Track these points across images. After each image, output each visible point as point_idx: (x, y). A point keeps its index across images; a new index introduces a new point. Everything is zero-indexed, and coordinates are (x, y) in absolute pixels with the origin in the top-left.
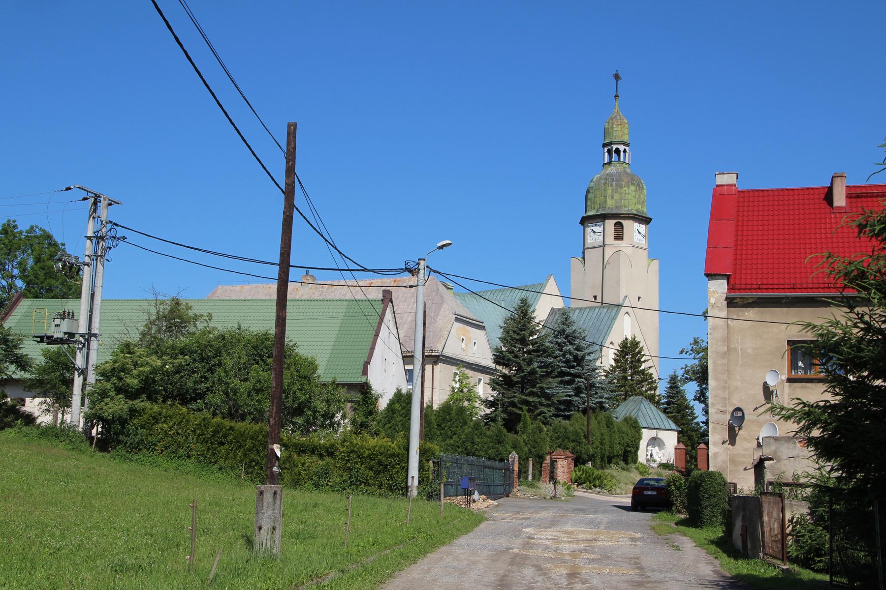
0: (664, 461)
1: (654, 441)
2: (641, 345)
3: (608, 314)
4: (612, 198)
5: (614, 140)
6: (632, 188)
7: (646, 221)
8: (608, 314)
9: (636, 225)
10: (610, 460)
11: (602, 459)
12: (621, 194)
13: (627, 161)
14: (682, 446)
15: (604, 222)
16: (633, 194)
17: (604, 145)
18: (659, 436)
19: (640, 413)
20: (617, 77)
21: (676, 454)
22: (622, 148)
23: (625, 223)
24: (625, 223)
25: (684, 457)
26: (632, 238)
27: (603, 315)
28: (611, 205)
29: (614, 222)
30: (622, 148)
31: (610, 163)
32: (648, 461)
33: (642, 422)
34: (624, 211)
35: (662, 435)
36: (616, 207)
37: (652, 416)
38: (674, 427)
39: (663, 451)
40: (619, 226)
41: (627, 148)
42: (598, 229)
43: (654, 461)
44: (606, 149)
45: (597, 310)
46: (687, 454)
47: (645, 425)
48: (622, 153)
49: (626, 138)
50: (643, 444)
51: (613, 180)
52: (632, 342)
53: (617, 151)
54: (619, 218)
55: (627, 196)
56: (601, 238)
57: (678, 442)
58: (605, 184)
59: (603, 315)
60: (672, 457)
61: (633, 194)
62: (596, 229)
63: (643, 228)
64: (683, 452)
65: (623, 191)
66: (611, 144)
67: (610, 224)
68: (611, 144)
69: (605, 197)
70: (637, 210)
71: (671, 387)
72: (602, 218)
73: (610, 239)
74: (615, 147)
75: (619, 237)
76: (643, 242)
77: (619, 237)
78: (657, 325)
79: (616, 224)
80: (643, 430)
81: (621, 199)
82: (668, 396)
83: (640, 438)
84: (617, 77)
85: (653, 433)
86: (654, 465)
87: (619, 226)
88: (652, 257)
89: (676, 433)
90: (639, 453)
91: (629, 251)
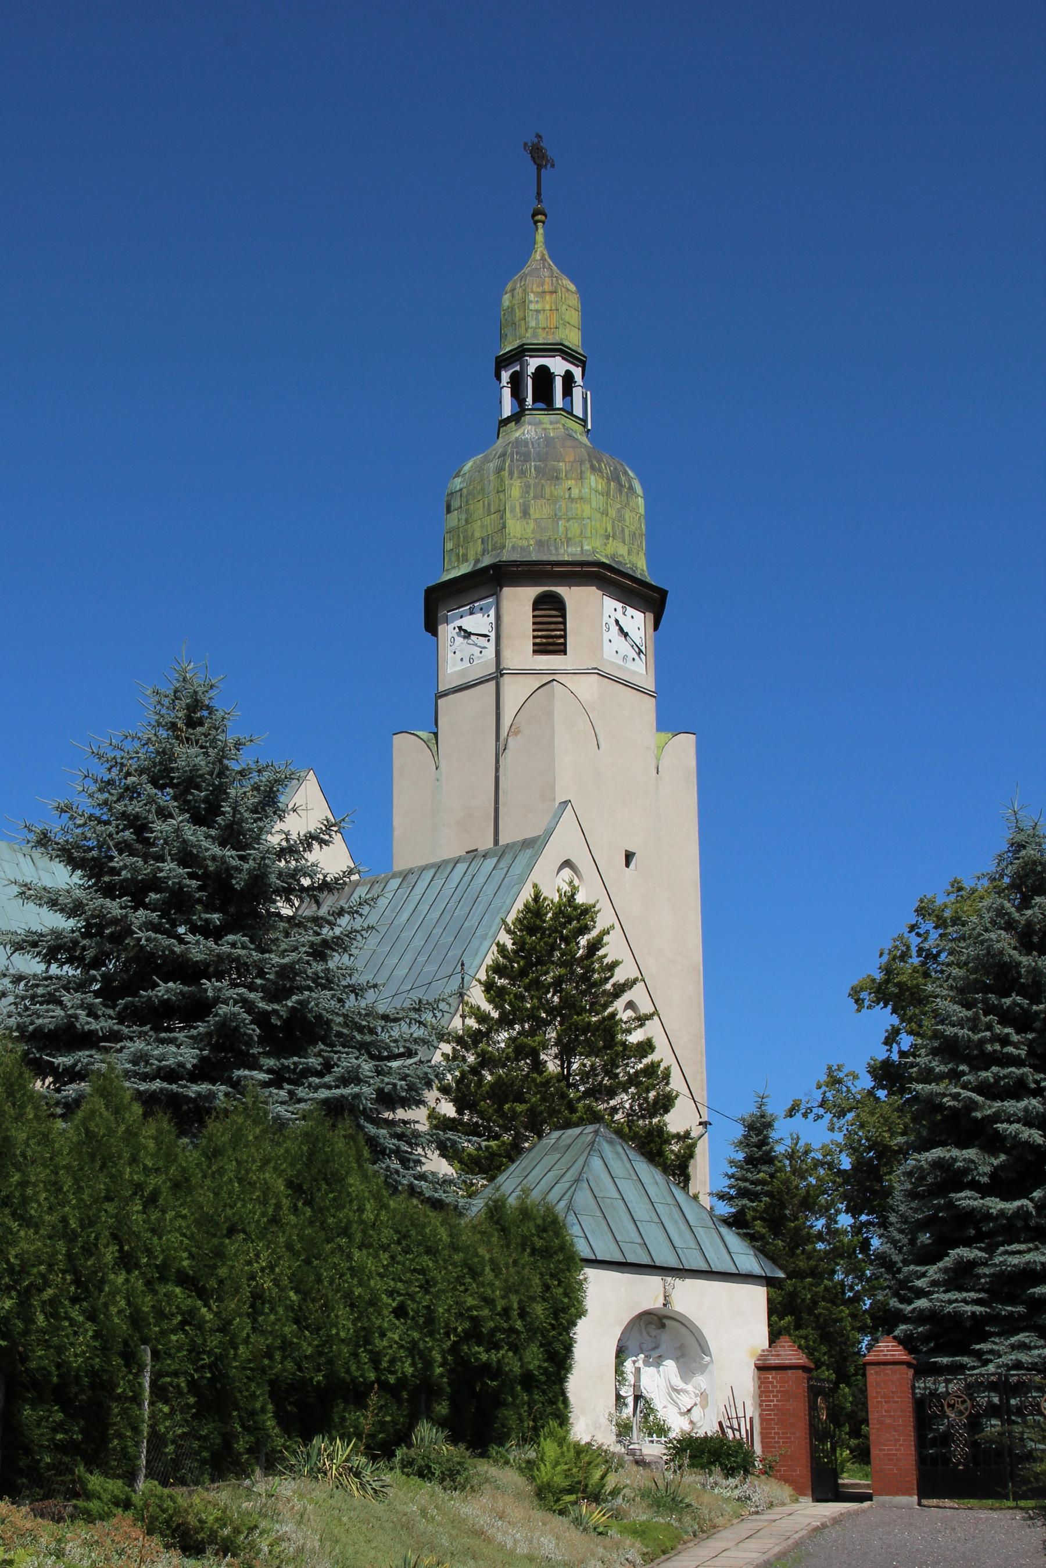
0: (707, 1426)
1: (654, 1332)
2: (603, 920)
3: (498, 875)
4: (526, 513)
5: (529, 338)
6: (594, 481)
7: (649, 598)
8: (498, 875)
9: (611, 606)
10: (310, 1410)
11: (213, 1397)
12: (554, 500)
13: (578, 411)
14: (789, 1353)
15: (496, 594)
16: (597, 501)
17: (502, 362)
18: (680, 1306)
19: (583, 1197)
20: (538, 156)
21: (763, 1391)
22: (558, 366)
23: (574, 596)
24: (574, 596)
25: (799, 1406)
26: (598, 647)
27: (480, 880)
28: (521, 539)
29: (529, 593)
30: (558, 366)
31: (516, 417)
32: (624, 1430)
33: (586, 1235)
34: (568, 553)
35: (691, 1298)
36: (540, 543)
37: (641, 1210)
38: (749, 1261)
39: (701, 1381)
40: (550, 607)
41: (577, 372)
42: (479, 622)
43: (661, 1430)
44: (505, 376)
45: (461, 868)
46: (814, 1392)
47: (605, 1250)
48: (558, 383)
49: (573, 339)
50: (593, 1342)
51: (526, 457)
52: (559, 912)
53: (544, 376)
54: (550, 579)
55: (578, 508)
56: (490, 653)
57: (774, 1336)
58: (499, 470)
59: (480, 880)
60: (748, 1405)
61: (597, 501)
62: (470, 623)
63: (636, 621)
64: (797, 1382)
65: (560, 490)
66: (520, 353)
67: (518, 602)
68: (520, 353)
69: (501, 512)
70: (613, 557)
71: (749, 1160)
72: (490, 580)
73: (520, 651)
74: (533, 364)
75: (551, 640)
76: (641, 671)
77: (551, 640)
78: (698, 956)
79: (539, 603)
80: (591, 1274)
81: (556, 518)
82: (743, 1193)
83: (566, 1310)
84: (538, 156)
85: (646, 1292)
86: (653, 1449)
87: (550, 607)
88: (669, 722)
89: (757, 1297)
90: (575, 1385)
91: (588, 688)
